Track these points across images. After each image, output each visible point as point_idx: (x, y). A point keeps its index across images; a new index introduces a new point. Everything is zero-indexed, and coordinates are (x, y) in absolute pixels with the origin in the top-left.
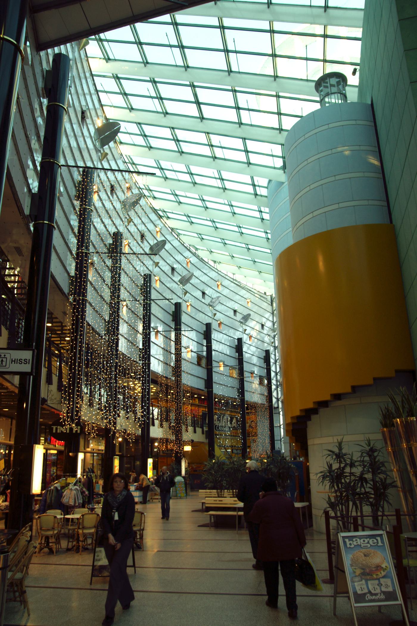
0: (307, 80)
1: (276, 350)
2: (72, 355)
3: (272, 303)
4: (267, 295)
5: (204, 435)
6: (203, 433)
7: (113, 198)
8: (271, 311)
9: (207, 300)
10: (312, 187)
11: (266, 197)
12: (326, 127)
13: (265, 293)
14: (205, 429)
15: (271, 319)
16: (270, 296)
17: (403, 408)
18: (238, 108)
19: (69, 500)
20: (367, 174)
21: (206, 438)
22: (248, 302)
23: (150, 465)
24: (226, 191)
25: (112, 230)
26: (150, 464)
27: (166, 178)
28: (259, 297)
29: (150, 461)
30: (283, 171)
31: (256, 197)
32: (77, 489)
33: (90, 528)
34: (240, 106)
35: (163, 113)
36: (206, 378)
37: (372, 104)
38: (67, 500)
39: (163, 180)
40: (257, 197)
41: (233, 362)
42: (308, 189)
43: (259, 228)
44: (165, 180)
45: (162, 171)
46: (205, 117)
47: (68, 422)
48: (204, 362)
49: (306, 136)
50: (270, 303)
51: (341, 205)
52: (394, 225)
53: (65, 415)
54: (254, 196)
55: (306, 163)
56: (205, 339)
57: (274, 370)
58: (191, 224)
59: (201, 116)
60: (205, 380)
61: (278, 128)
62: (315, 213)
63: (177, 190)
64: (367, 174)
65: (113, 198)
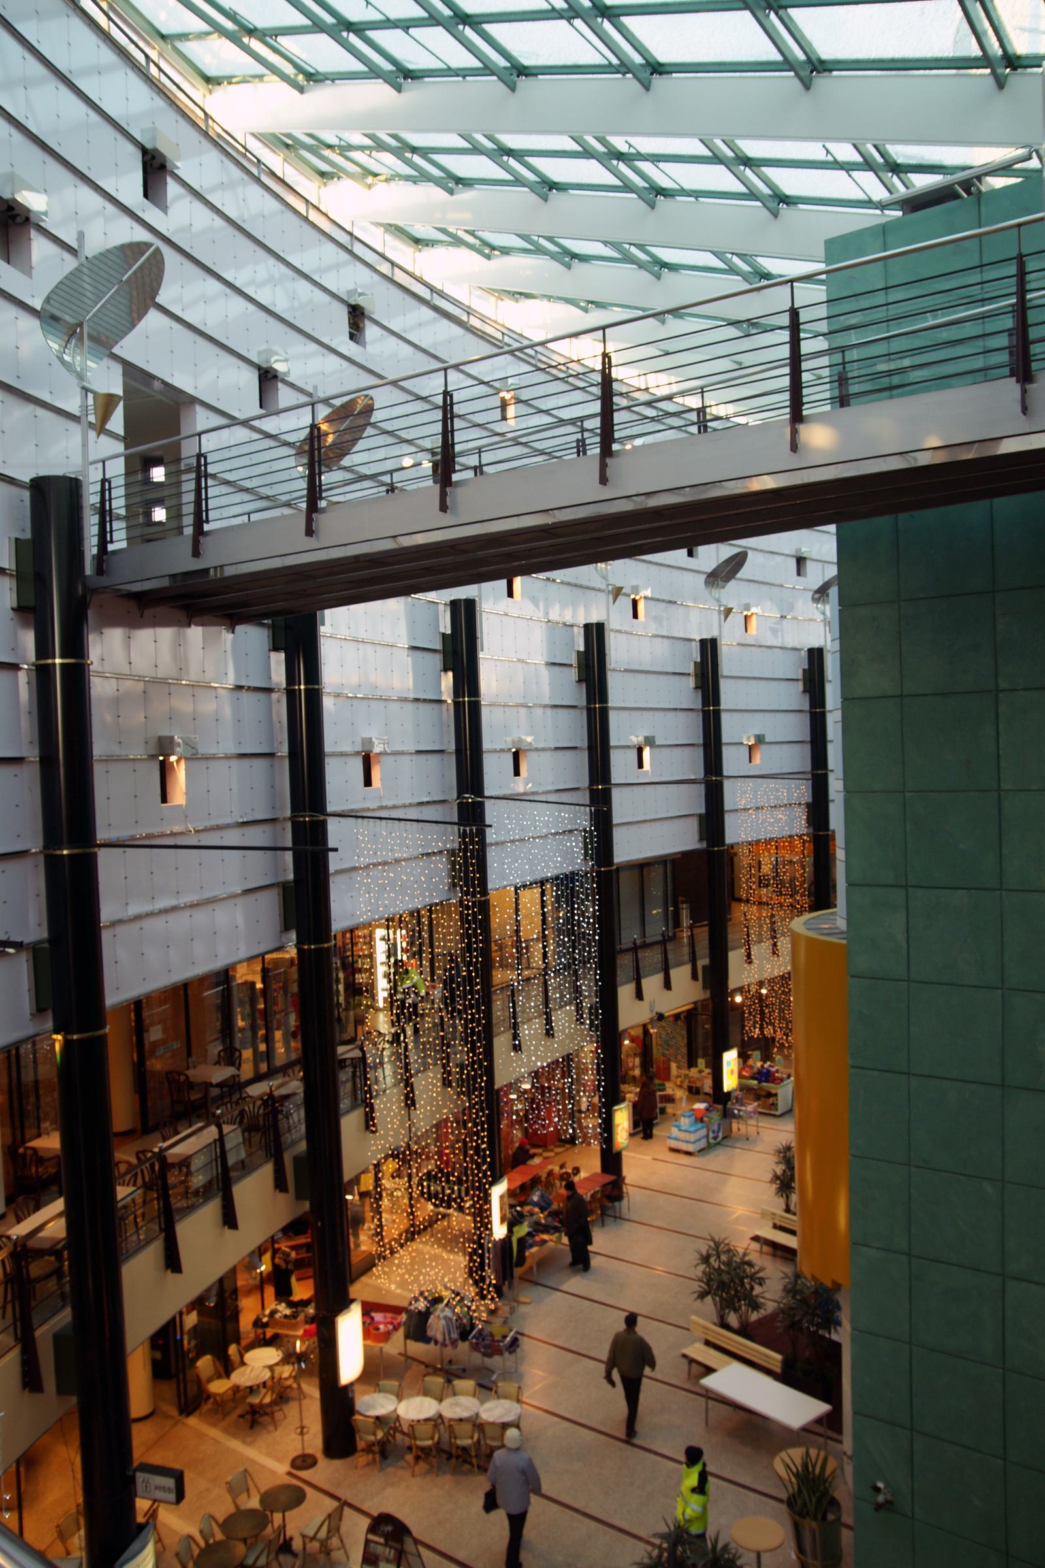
5: (700, 983)
6: (694, 976)
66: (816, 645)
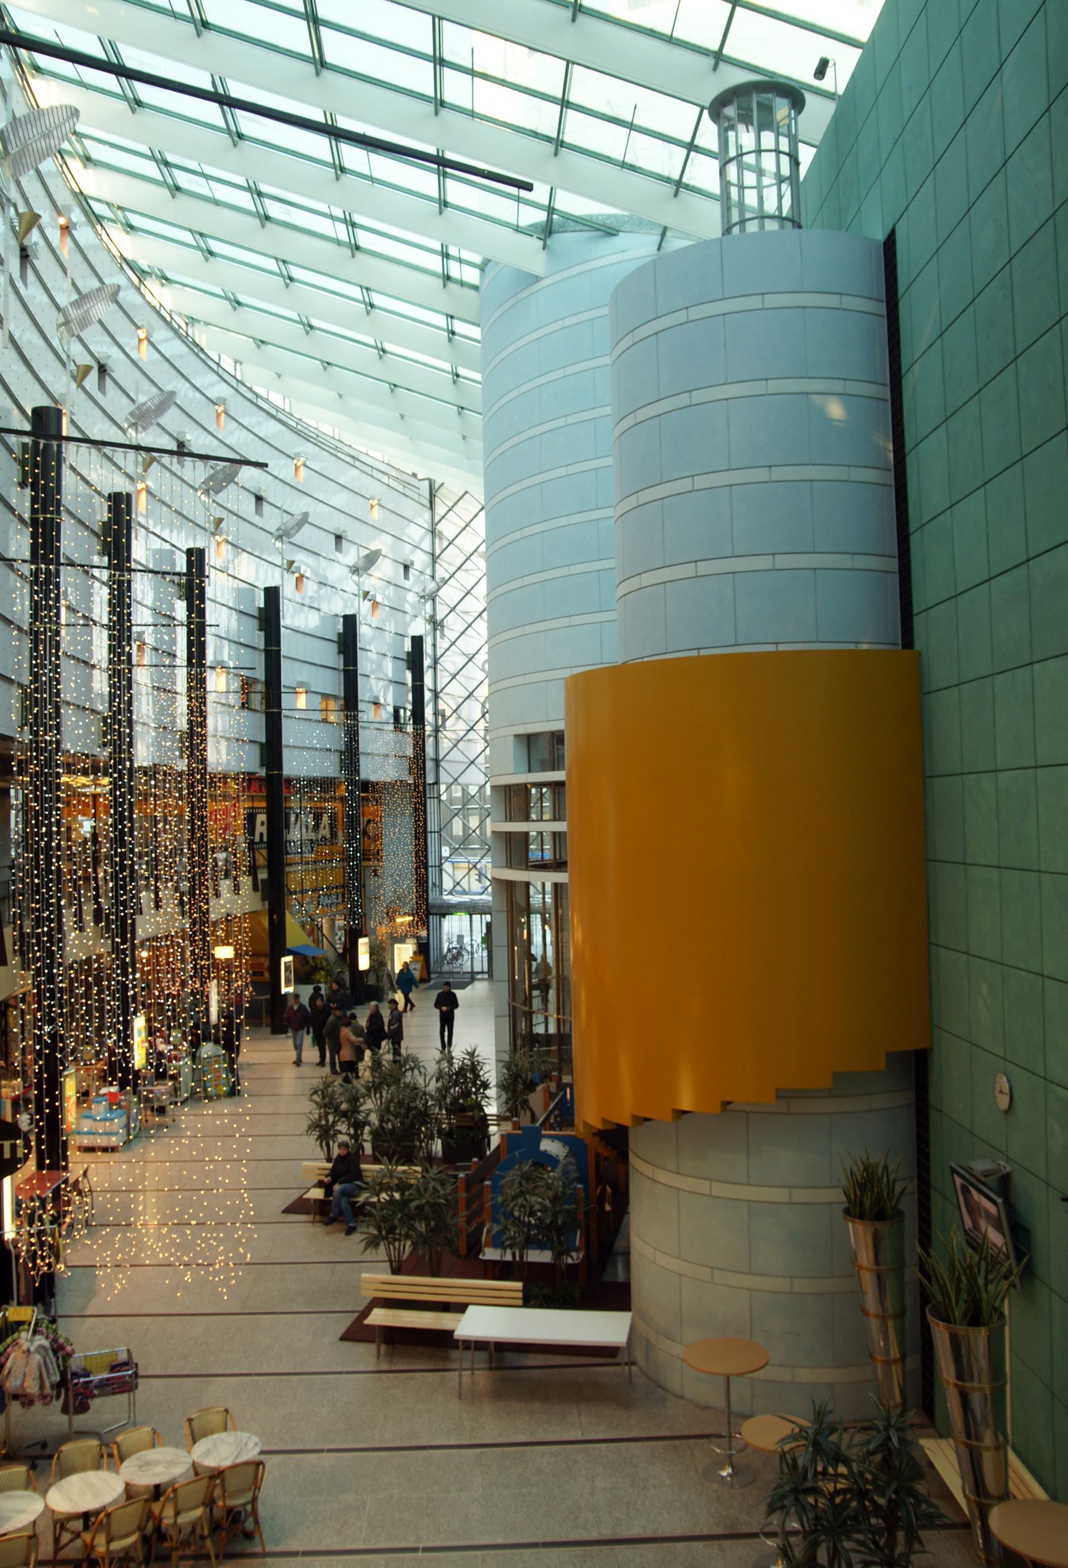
0: (670, 40)
1: (438, 632)
2: (40, 1067)
3: (431, 503)
4: (420, 477)
5: (259, 894)
6: (255, 888)
7: (26, 285)
8: (427, 526)
9: (272, 519)
10: (701, 482)
11: (475, 288)
12: (754, 302)
13: (414, 475)
14: (263, 875)
15: (427, 545)
16: (427, 482)
17: (958, 1290)
18: (439, 62)
19: (24, 1381)
20: (858, 474)
21: (263, 899)
22: (372, 506)
23: (140, 1035)
24: (358, 254)
25: (33, 399)
26: (139, 1031)
27: (176, 189)
28: (400, 488)
29: (139, 1023)
30: (541, 243)
31: (445, 286)
32: (42, 1347)
33: (127, 1535)
34: (447, 56)
35: (192, 20)
36: (263, 740)
37: (890, 245)
38: (19, 1382)
39: (166, 193)
40: (450, 285)
41: (334, 684)
42: (685, 485)
43: (439, 358)
44: (173, 197)
45: (165, 170)
46: (329, 58)
47: (43, 1258)
48: (257, 701)
49: (695, 313)
50: (428, 505)
51: (782, 561)
52: (919, 654)
53: (33, 1240)
54: (440, 282)
55: (683, 400)
56: (260, 630)
57: (431, 686)
58: (235, 309)
59: (317, 56)
60: (261, 744)
61: (555, 135)
62: (704, 568)
63: (123, 42)
64: (858, 474)
65: (26, 285)
66: (417, 634)
